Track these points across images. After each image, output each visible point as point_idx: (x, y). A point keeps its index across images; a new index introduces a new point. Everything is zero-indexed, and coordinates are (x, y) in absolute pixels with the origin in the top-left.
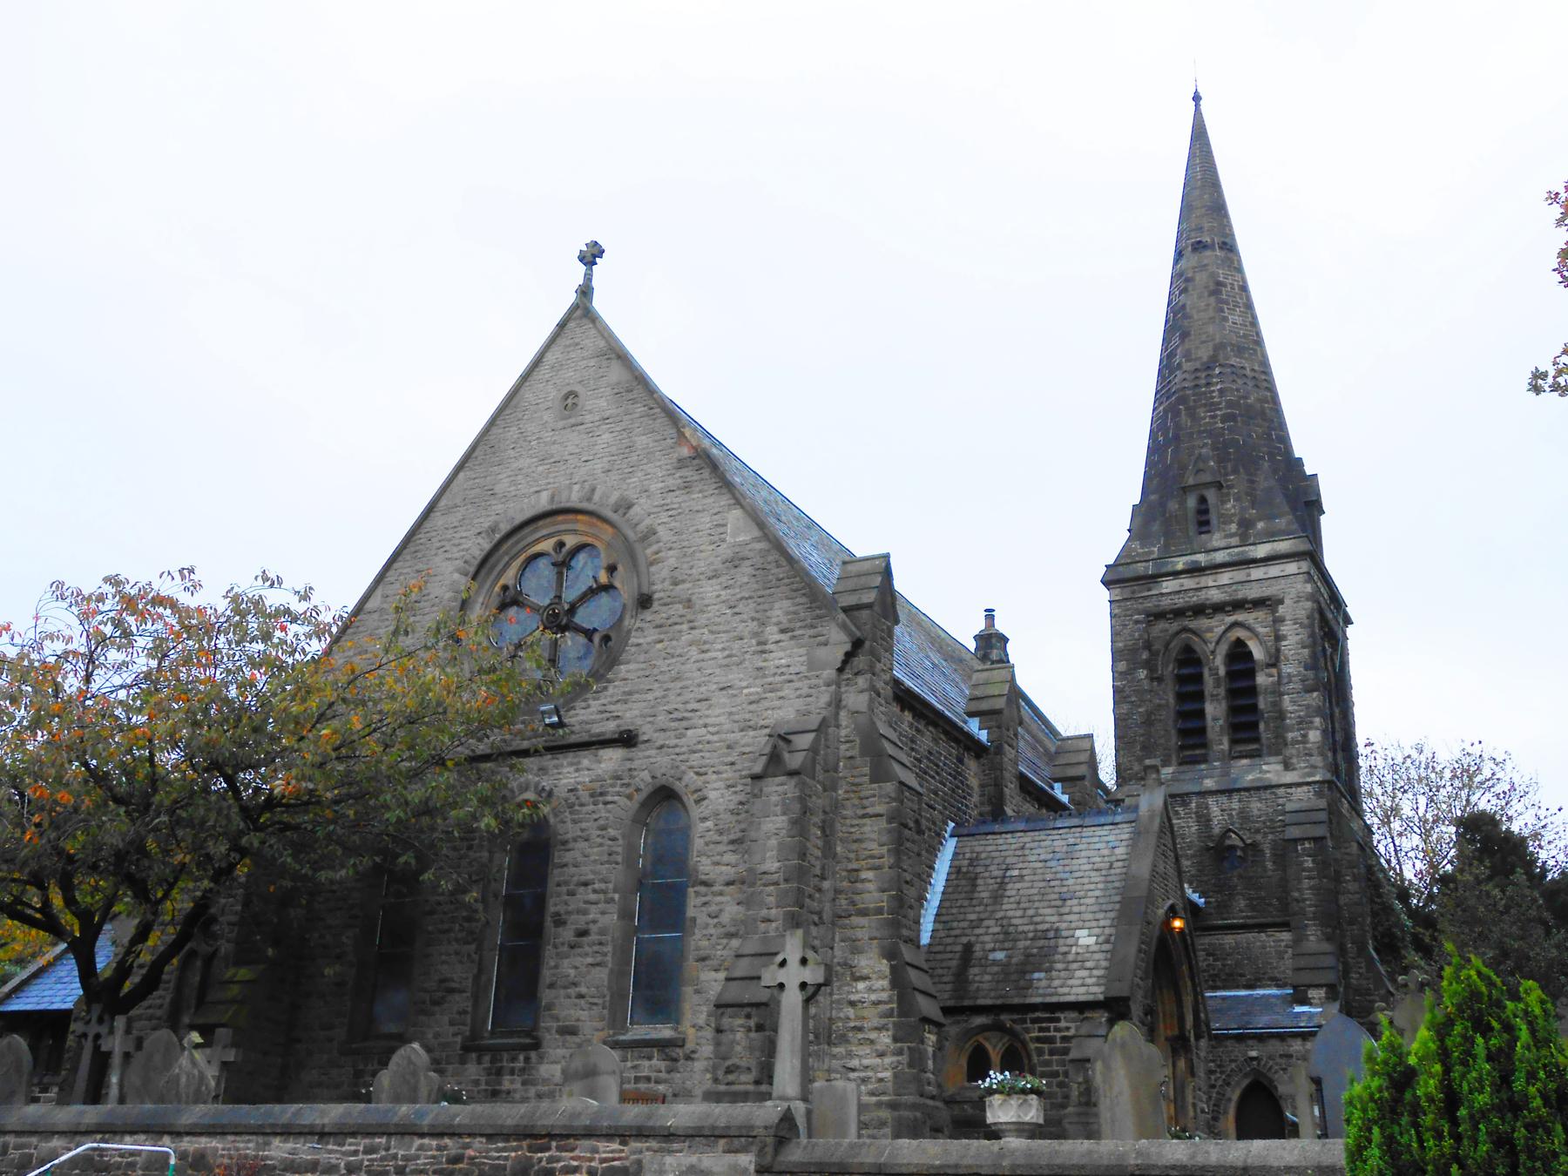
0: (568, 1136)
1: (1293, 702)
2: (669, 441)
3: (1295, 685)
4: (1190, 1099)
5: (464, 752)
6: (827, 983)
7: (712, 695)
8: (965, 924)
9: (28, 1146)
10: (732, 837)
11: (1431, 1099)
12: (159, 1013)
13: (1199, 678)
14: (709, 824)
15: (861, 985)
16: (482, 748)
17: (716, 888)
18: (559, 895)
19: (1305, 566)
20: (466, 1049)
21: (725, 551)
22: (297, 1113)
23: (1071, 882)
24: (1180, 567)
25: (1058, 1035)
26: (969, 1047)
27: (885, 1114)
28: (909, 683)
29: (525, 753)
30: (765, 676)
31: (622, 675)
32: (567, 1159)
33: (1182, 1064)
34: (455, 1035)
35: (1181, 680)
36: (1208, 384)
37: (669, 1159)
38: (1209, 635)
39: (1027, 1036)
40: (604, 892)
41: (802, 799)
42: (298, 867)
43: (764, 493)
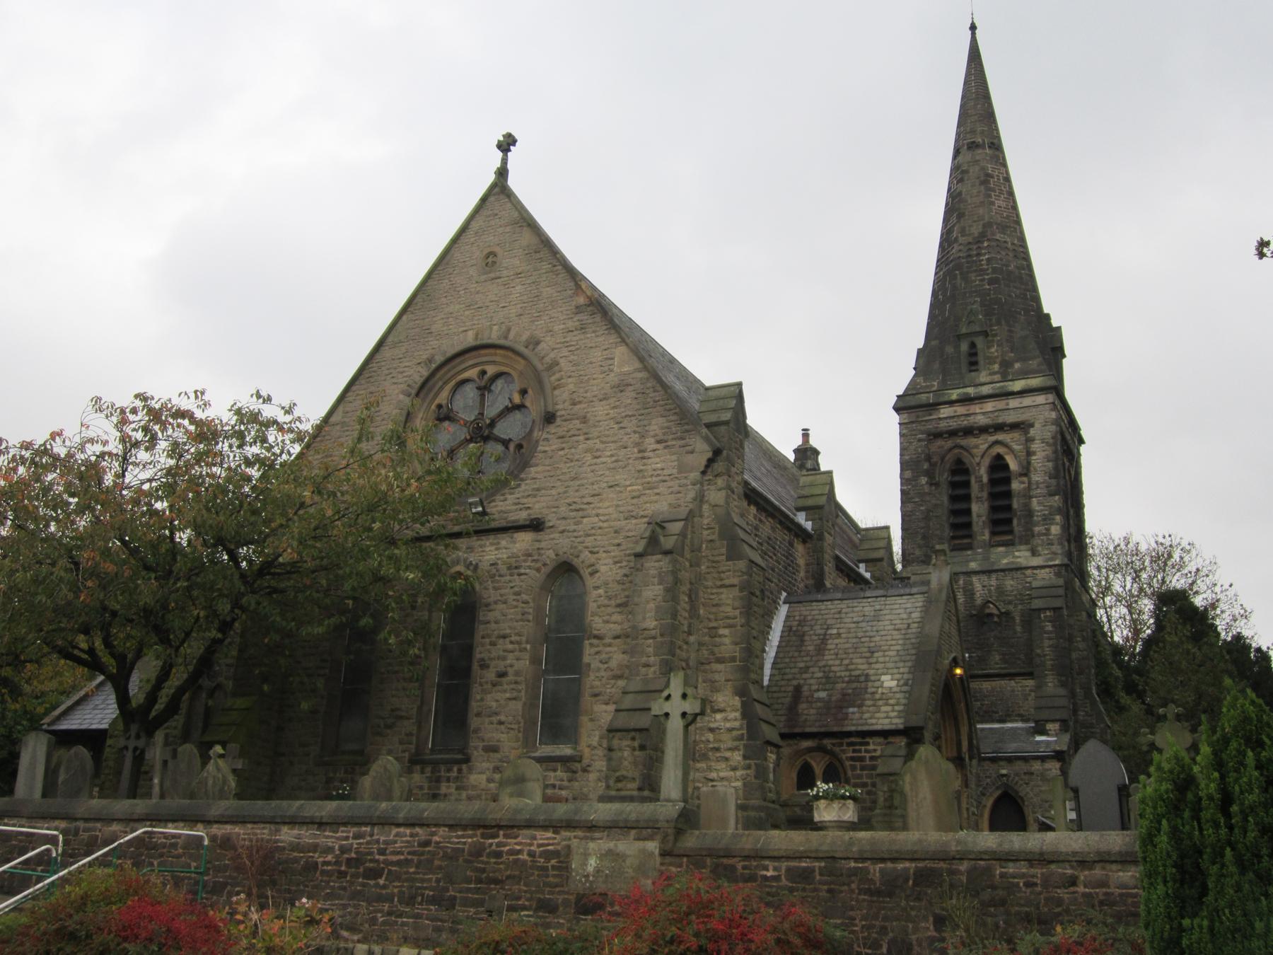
0: (512, 827)
1: (1039, 503)
2: (570, 292)
4: (964, 805)
5: (410, 534)
7: (600, 493)
8: (796, 670)
9: (94, 829)
10: (619, 601)
11: (1211, 798)
13: (967, 484)
14: (601, 591)
15: (718, 716)
16: (424, 531)
17: (607, 641)
18: (483, 645)
19: (1051, 397)
21: (613, 378)
23: (877, 638)
24: (954, 397)
25: (868, 755)
26: (799, 763)
28: (754, 484)
29: (458, 535)
30: (644, 477)
31: (532, 475)
32: (512, 844)
34: (404, 751)
35: (954, 485)
36: (979, 255)
37: (592, 845)
38: (975, 451)
39: (844, 757)
40: (519, 643)
42: (284, 623)
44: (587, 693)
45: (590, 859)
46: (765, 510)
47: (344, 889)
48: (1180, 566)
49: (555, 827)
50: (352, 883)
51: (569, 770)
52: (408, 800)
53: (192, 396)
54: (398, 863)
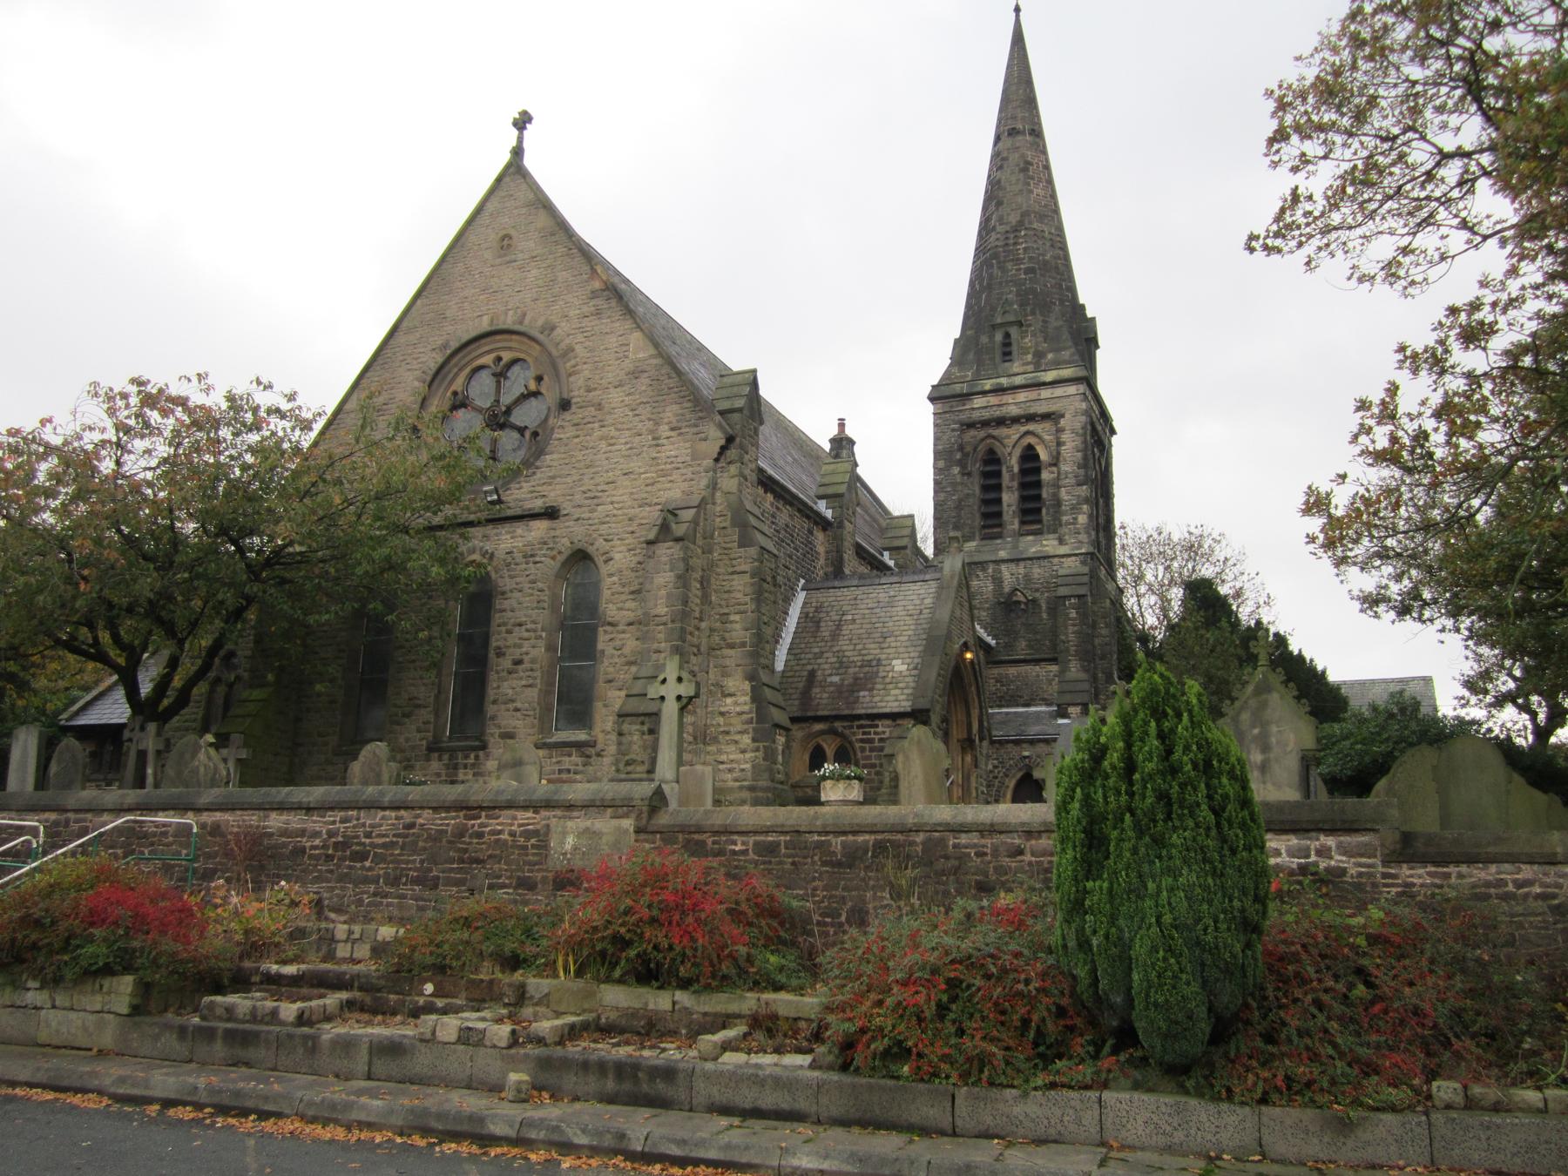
0: (494, 808)
1: (1068, 493)
3: (1071, 481)
4: (974, 785)
6: (697, 695)
7: (616, 479)
9: (84, 820)
12: (194, 725)
13: (998, 474)
14: (615, 579)
15: (729, 700)
16: (438, 520)
17: (621, 628)
19: (1082, 388)
20: (430, 749)
21: (628, 365)
22: (288, 794)
24: (987, 387)
26: (811, 746)
27: (746, 795)
28: (771, 472)
29: (471, 524)
32: (494, 825)
33: (968, 758)
35: (985, 475)
37: (570, 824)
41: (685, 560)
43: (663, 322)
44: (601, 678)
45: (567, 839)
46: (783, 498)
47: (331, 872)
48: (1207, 557)
49: (535, 806)
50: (338, 866)
51: (584, 755)
52: (396, 784)
53: (195, 380)
54: (384, 846)
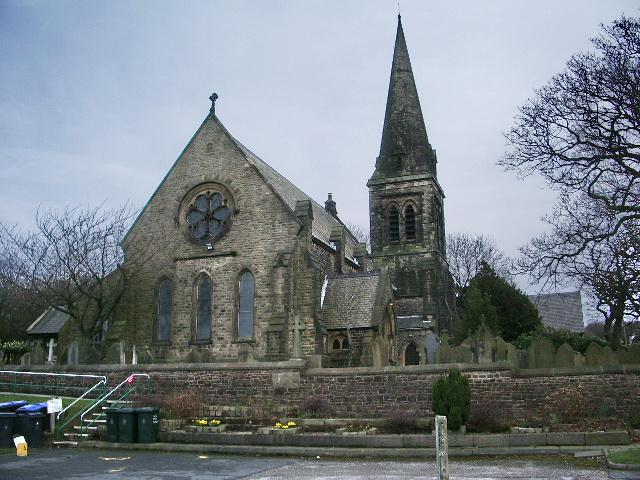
13: (397, 218)
